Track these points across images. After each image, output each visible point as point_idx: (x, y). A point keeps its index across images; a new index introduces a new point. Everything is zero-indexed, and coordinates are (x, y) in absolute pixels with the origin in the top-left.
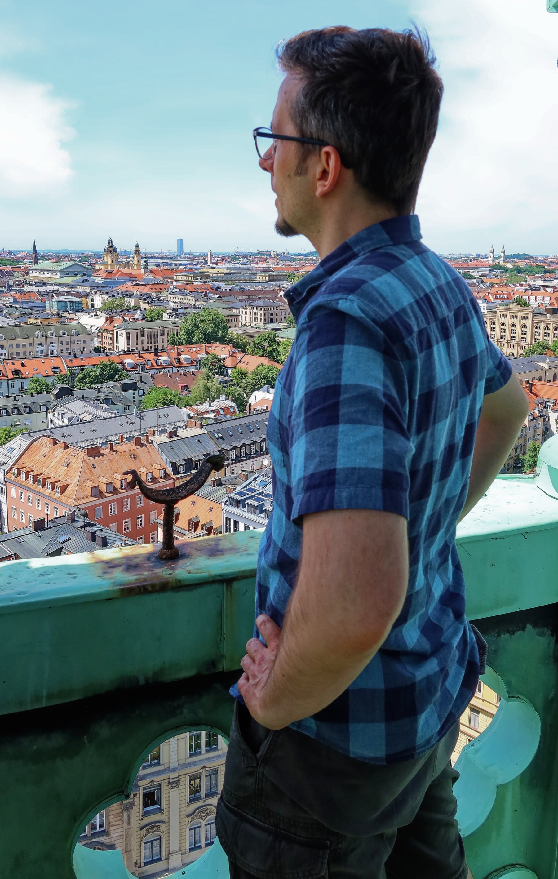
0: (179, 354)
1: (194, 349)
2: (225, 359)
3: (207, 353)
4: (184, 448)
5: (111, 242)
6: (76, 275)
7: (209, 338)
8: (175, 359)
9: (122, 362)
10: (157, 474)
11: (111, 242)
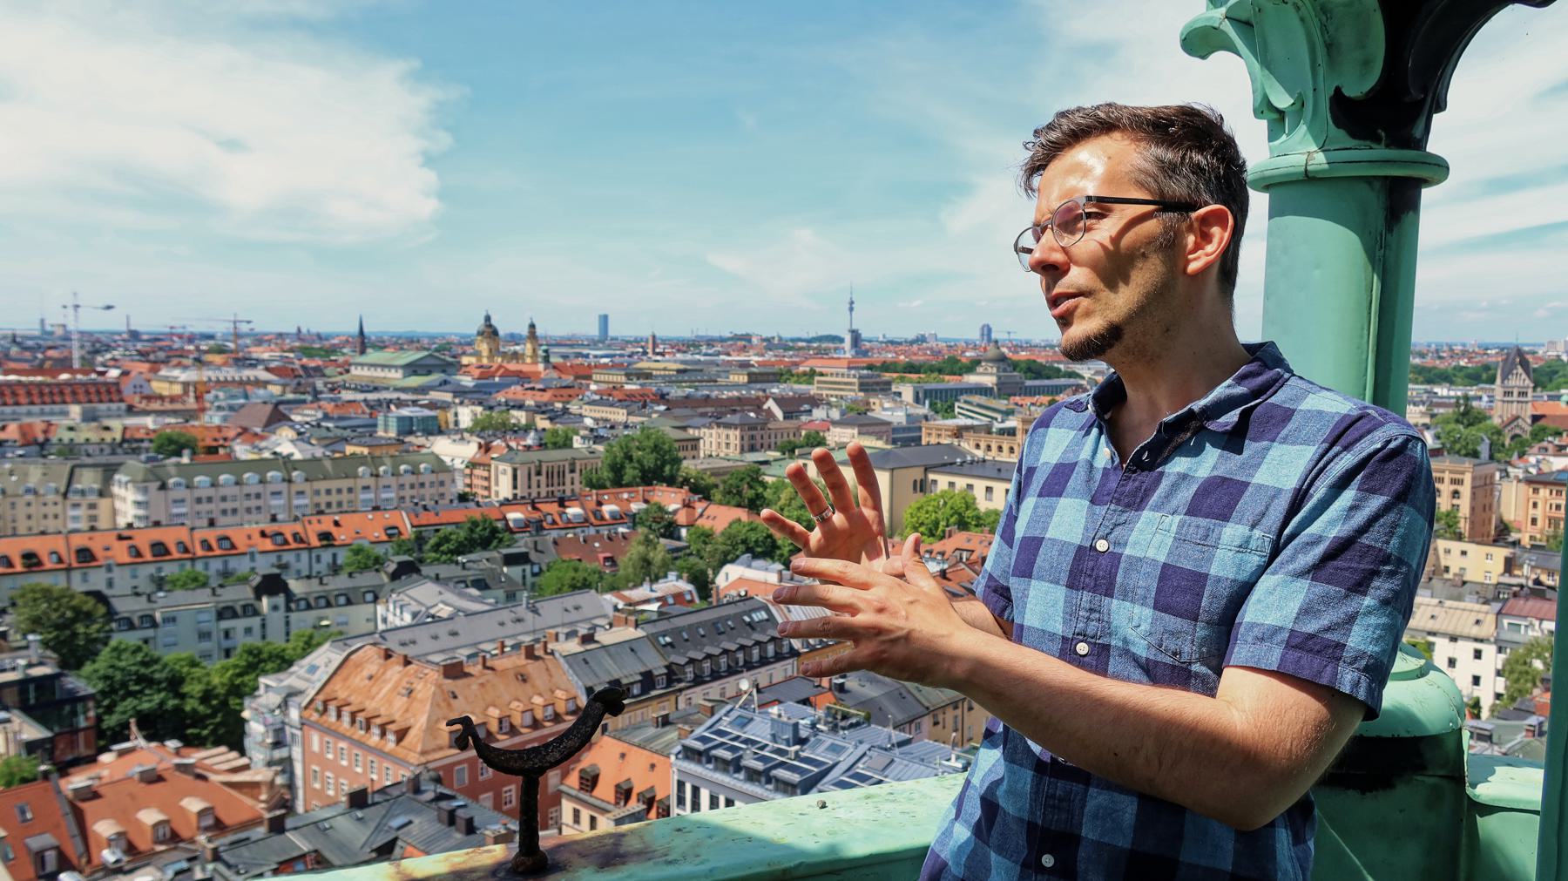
0: (600, 504)
1: (625, 496)
2: (675, 512)
3: (646, 501)
4: (608, 662)
5: (488, 318)
6: (429, 373)
7: (650, 477)
8: (594, 514)
9: (505, 519)
10: (561, 708)
11: (488, 318)
